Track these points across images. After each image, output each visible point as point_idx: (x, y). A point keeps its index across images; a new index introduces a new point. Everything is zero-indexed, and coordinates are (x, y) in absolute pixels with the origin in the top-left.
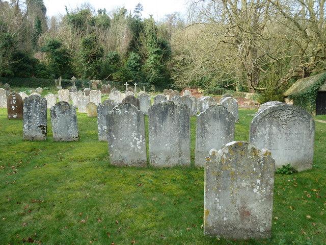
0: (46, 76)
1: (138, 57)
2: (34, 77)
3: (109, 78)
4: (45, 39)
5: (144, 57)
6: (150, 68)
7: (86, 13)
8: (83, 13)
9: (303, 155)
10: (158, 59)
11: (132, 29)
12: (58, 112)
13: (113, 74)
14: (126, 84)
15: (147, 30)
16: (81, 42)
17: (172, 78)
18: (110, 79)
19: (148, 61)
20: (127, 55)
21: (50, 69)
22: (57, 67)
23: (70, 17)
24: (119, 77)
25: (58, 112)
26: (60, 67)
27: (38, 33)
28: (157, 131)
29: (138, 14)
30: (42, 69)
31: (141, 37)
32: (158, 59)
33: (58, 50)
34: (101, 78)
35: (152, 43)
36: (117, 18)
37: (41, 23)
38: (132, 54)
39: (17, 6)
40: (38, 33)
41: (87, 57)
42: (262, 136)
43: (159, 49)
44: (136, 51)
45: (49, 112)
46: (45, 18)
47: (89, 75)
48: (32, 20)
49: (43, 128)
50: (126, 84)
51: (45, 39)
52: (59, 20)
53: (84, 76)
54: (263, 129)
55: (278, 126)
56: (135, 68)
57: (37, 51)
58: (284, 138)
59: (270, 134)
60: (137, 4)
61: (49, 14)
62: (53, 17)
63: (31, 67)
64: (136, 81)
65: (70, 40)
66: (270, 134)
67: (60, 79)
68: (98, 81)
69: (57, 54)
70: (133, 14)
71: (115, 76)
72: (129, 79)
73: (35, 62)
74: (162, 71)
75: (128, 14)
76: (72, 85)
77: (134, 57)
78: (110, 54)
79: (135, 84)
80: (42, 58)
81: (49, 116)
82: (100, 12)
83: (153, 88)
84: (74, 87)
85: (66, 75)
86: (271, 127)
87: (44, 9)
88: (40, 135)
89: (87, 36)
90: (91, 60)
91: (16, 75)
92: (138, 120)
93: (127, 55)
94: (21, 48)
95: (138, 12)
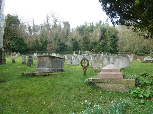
0: (70, 51)
1: (104, 42)
2: (66, 51)
3: (92, 50)
4: (70, 38)
5: (106, 42)
6: (109, 46)
7: (84, 27)
8: (83, 27)
9: (127, 66)
10: (112, 42)
11: (102, 31)
12: (74, 58)
13: (94, 49)
14: (99, 53)
15: (107, 31)
16: (82, 38)
17: (117, 49)
18: (93, 51)
19: (108, 43)
20: (100, 41)
21: (72, 48)
22: (73, 47)
23: (79, 29)
24: (96, 50)
25: (74, 58)
26: (75, 47)
27: (67, 35)
28: (33, 18)
29: (107, 22)
30: (69, 48)
31: (105, 33)
32: (112, 42)
33: (74, 41)
34: (89, 51)
35: (109, 36)
36: (98, 25)
37: (68, 31)
38: (102, 41)
39: (60, 26)
40: (67, 35)
41: (84, 43)
42: (116, 61)
43: (113, 38)
44: (104, 40)
45: (72, 59)
46: (70, 29)
47: (85, 50)
48: (66, 31)
49: (71, 62)
50: (99, 53)
51: (70, 38)
52: (75, 29)
53: (83, 50)
54: (116, 60)
55: (120, 59)
56: (103, 46)
57: (67, 41)
58: (122, 62)
59: (118, 61)
60: (107, 19)
61: (71, 28)
62: (72, 28)
63: (65, 47)
64: (103, 51)
65: (78, 37)
66: (118, 61)
67: (75, 51)
68: (88, 52)
69: (74, 42)
70: (105, 23)
71: (95, 49)
72: (100, 51)
73: (66, 46)
74: (114, 47)
75: (102, 23)
76: (79, 53)
77: (102, 42)
78: (92, 41)
79: (103, 53)
80: (69, 44)
81: (72, 59)
82: (91, 24)
83: (110, 54)
84: (79, 54)
85: (77, 50)
86: (118, 59)
87: (69, 26)
88: (70, 64)
89: (84, 36)
90: (86, 44)
91: (61, 50)
92: (90, 58)
93: (100, 41)
94: (62, 41)
95: (107, 22)
